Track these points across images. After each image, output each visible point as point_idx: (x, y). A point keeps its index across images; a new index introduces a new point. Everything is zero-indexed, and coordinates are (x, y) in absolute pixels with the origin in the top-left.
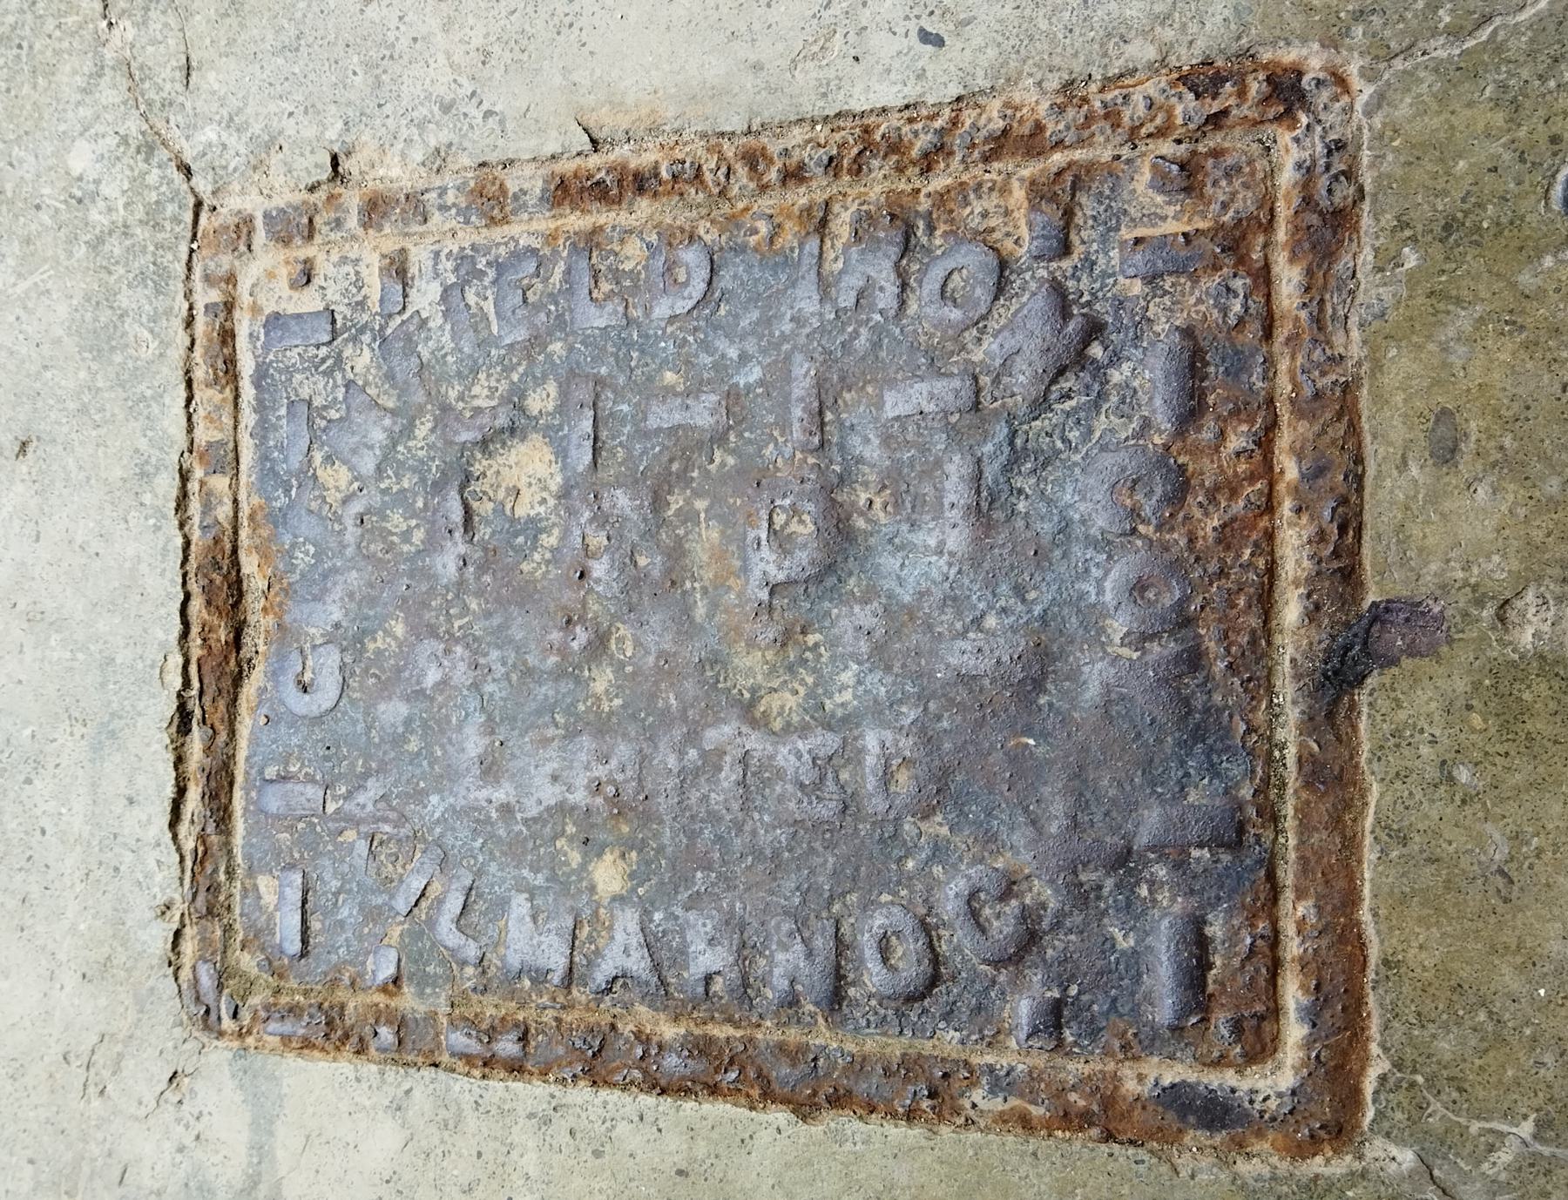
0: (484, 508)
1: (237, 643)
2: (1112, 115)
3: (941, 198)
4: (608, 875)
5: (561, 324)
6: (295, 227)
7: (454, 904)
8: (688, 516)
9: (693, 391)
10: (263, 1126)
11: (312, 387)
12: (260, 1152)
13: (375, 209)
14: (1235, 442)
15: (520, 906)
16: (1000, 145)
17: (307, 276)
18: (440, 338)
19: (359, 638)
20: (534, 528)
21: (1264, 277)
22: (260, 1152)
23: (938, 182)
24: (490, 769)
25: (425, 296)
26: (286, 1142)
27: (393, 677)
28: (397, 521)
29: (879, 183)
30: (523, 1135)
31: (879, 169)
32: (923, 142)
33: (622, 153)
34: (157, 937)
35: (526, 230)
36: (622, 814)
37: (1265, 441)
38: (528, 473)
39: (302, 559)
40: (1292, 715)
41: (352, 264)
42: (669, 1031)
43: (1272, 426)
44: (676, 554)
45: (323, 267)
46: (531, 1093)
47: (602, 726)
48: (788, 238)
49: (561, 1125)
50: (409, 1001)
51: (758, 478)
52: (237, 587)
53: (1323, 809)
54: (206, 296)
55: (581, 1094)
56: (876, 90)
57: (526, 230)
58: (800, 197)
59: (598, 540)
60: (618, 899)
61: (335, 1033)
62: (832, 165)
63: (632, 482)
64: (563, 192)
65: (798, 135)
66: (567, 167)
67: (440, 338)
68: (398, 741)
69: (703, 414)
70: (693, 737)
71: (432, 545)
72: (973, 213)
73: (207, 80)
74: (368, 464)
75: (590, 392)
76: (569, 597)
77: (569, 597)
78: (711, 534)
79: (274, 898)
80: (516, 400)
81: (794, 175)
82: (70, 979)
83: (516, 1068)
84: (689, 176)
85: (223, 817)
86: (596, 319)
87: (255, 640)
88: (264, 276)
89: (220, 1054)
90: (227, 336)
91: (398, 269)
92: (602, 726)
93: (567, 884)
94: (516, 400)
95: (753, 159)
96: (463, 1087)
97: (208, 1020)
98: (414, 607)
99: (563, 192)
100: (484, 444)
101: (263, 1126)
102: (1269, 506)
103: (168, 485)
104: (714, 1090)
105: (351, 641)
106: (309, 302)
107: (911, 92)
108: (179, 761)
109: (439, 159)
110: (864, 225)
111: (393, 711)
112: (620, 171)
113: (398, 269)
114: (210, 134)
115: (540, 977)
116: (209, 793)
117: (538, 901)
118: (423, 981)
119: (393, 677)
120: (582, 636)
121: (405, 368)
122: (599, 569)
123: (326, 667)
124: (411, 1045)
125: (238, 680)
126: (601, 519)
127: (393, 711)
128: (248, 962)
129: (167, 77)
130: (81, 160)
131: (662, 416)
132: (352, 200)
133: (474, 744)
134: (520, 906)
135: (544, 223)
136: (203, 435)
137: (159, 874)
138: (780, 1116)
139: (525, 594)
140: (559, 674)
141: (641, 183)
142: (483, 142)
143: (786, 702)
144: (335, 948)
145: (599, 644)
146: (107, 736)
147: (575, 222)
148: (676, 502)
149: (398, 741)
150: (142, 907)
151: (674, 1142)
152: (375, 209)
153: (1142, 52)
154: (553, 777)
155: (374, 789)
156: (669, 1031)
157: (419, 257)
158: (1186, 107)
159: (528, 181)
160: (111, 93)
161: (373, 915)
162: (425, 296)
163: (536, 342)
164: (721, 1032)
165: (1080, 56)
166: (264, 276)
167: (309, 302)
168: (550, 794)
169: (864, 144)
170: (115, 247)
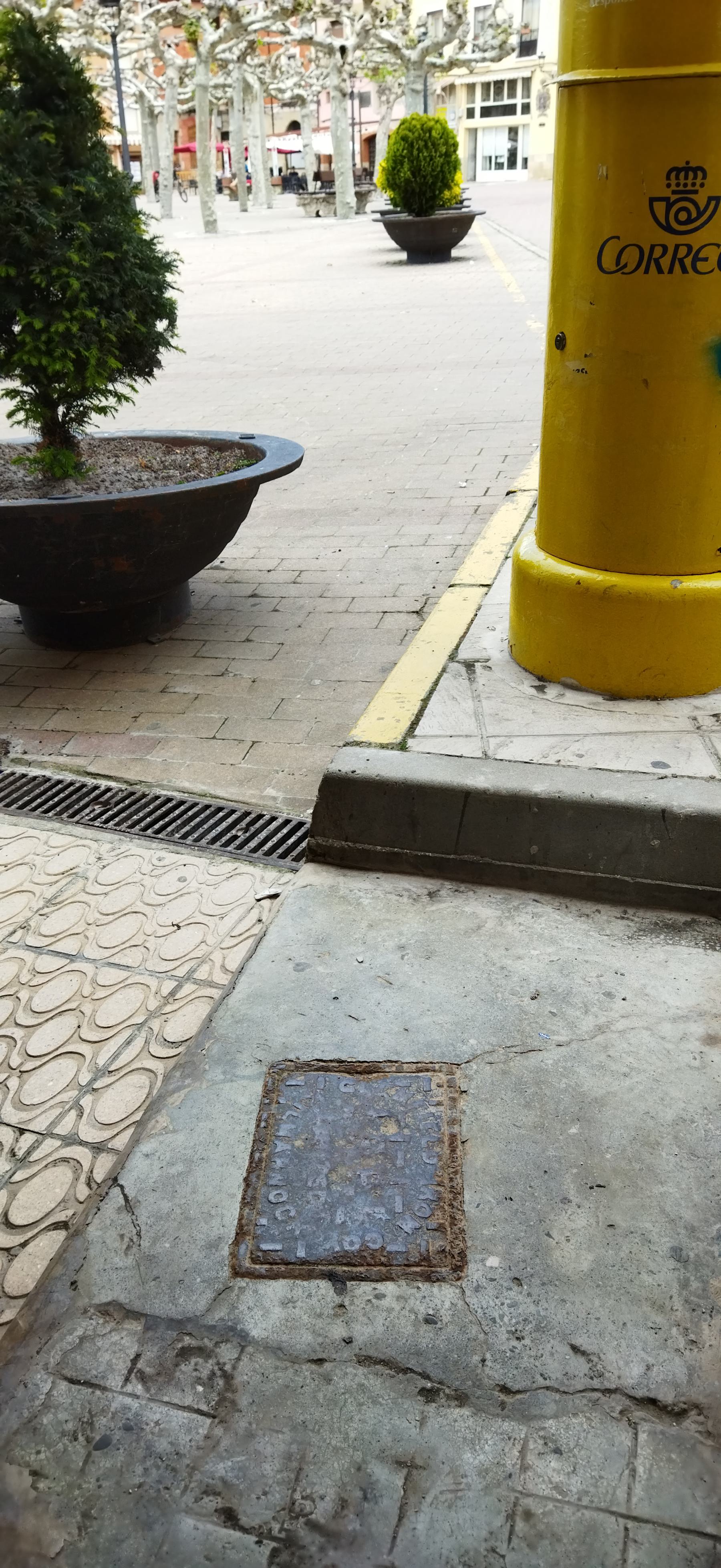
0: (383, 1120)
1: (357, 1073)
2: (456, 1238)
3: (443, 1207)
4: (298, 1143)
5: (423, 1135)
6: (451, 1084)
7: (295, 1114)
8: (377, 1159)
9: (405, 1160)
10: (249, 1078)
11: (414, 1087)
12: (244, 1077)
13: (453, 1100)
14: (383, 1259)
15: (293, 1127)
16: (453, 1218)
17: (439, 1086)
18: (422, 1112)
19: (357, 1097)
20: (378, 1130)
21: (417, 1265)
22: (244, 1077)
23: (446, 1207)
24: (323, 1121)
25: (432, 1109)
26: (245, 1082)
27: (346, 1102)
28: (382, 1103)
29: (448, 1196)
30: (244, 1127)
31: (451, 1196)
32: (455, 1204)
33: (460, 1147)
34: (292, 1057)
35: (445, 1129)
36: (311, 1145)
37: (382, 1264)
38: (391, 1129)
39: (375, 1085)
40: (324, 1268)
41: (441, 1095)
42: (264, 1155)
43: (386, 1266)
44: (369, 1157)
45: (441, 1090)
46: (252, 1128)
47: (332, 1142)
48: (437, 1179)
49: (245, 1134)
50: (274, 1106)
51: (384, 1172)
52: (370, 1073)
53: (303, 1272)
54: (437, 1066)
55: (252, 1138)
56: (467, 1196)
57: (445, 1129)
58: (446, 1181)
59: (374, 1142)
60: (293, 1145)
61: (267, 1092)
62: (452, 1187)
63: (386, 1148)
64: (453, 1136)
65: (460, 1181)
66: (459, 1137)
67: (422, 1112)
68: (332, 1103)
69: (400, 1162)
70: (327, 1159)
71: (375, 1110)
72: (439, 1213)
73: (488, 1067)
74: (395, 1098)
75: (409, 1140)
76: (361, 1136)
77: (361, 1136)
78: (373, 1164)
79: (299, 1079)
80: (407, 1126)
81: (451, 1180)
82: (284, 1040)
83: (258, 1126)
84: (453, 1159)
85: (317, 1070)
86: (423, 1142)
87: (358, 1076)
88: (442, 1078)
89: (265, 1069)
90: (427, 1070)
91: (439, 1104)
92: (332, 1142)
93: (297, 1135)
94: (407, 1126)
95: (456, 1173)
96: (255, 1115)
97: (272, 1066)
98: (362, 1106)
99: (453, 1136)
100: (397, 1120)
101: (249, 1078)
102: (369, 1265)
103: (395, 1058)
104: (251, 1163)
105: (355, 1095)
106: (433, 1086)
107: (467, 1202)
108: (331, 1061)
109: (463, 1112)
110: (439, 1193)
111: (339, 1102)
112: (457, 1147)
113: (439, 1104)
114: (475, 1067)
115: (278, 1130)
116: (324, 1066)
117: (315, 99)
118: (278, 1109)
119: (346, 1102)
120: (352, 1139)
121: (416, 1105)
122: (367, 1142)
123: (350, 1090)
124: (263, 1106)
125: (349, 1073)
126: (378, 1142)
127: (339, 1102)
128: (285, 1074)
129: (491, 1059)
130: (472, 1041)
131: (400, 1155)
132: (456, 1095)
133: (330, 1118)
134: (293, 1127)
135: (447, 1132)
136: (405, 1066)
137: (305, 1057)
138: (245, 1175)
139: (362, 1128)
140: (344, 1135)
141: (453, 1151)
142: (466, 1120)
143: (334, 1177)
144: (287, 1092)
145: (350, 1142)
146: (339, 1047)
147: (446, 1139)
148: (381, 1157)
149: (332, 1103)
150: (298, 1054)
151: (241, 1155)
152: (453, 1100)
153: (469, 1244)
154: (320, 1132)
155: (322, 1099)
156: (264, 1155)
157: (442, 1108)
158: (457, 1251)
159: (456, 1129)
160: (487, 1048)
161: (294, 1098)
162: (432, 1109)
163: (419, 1130)
164: (263, 1164)
165: (469, 1233)
166: (442, 1078)
167: (433, 1086)
168: (317, 1132)
169: (457, 1193)
170: (451, 1048)
